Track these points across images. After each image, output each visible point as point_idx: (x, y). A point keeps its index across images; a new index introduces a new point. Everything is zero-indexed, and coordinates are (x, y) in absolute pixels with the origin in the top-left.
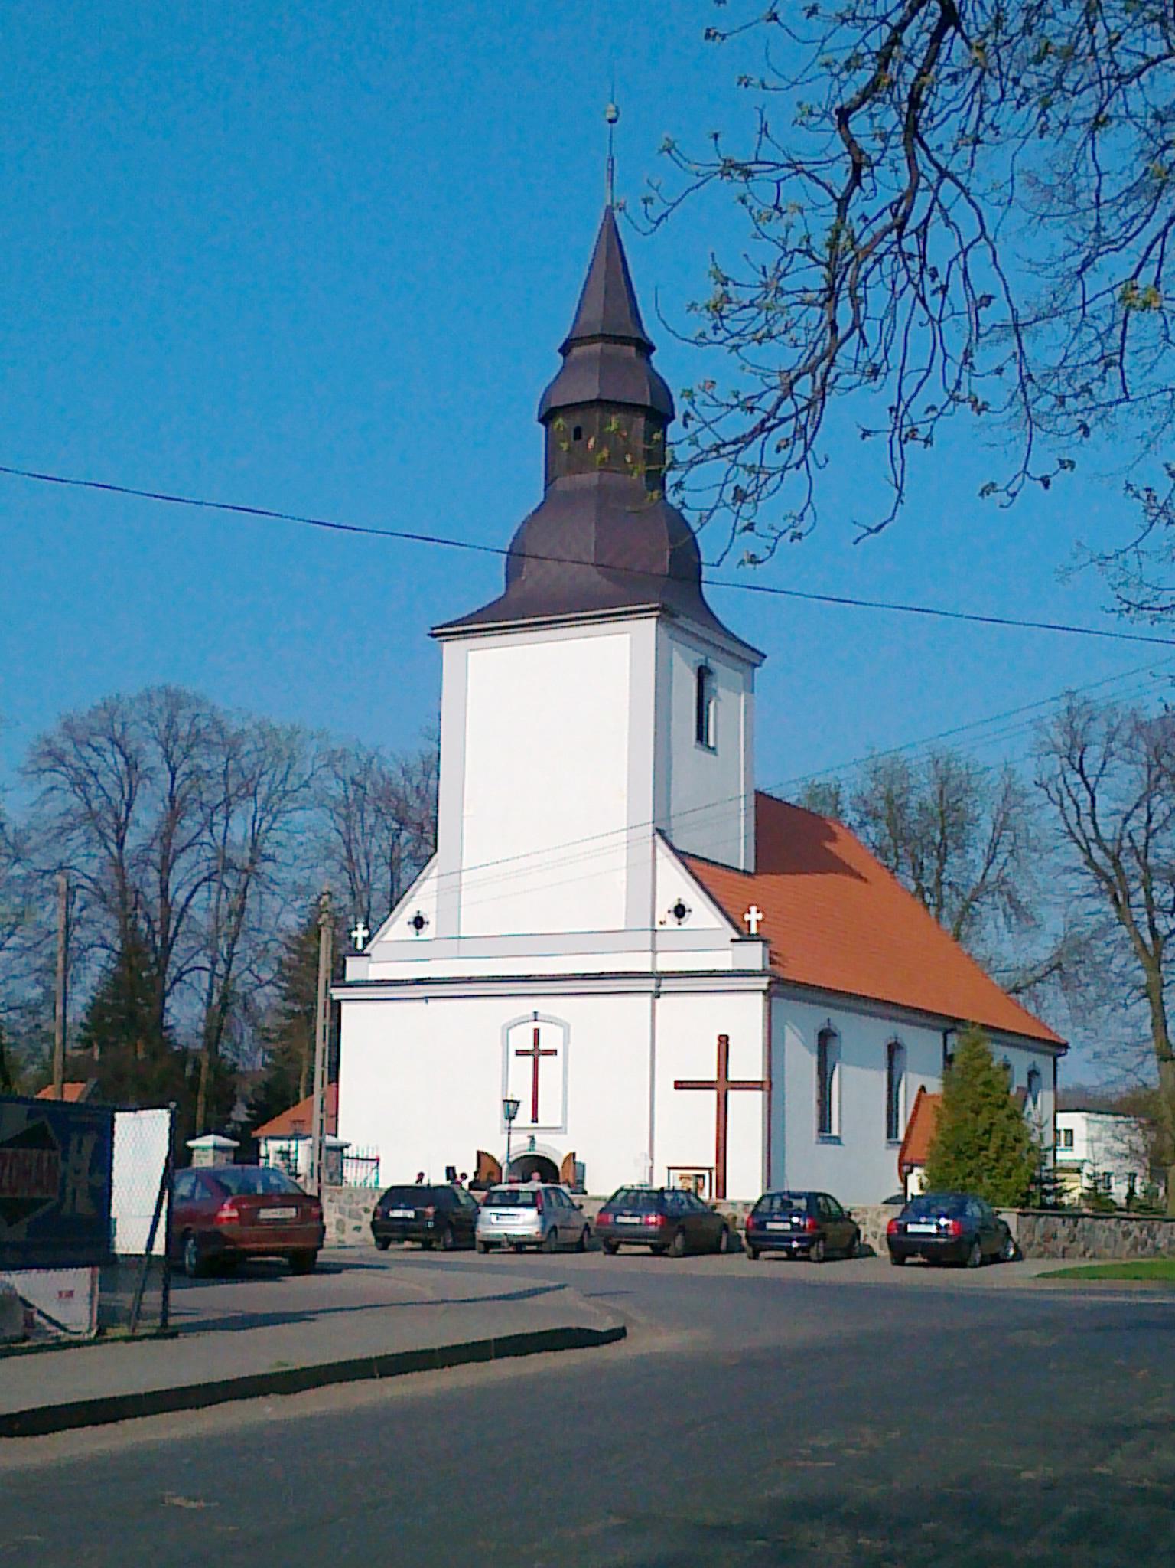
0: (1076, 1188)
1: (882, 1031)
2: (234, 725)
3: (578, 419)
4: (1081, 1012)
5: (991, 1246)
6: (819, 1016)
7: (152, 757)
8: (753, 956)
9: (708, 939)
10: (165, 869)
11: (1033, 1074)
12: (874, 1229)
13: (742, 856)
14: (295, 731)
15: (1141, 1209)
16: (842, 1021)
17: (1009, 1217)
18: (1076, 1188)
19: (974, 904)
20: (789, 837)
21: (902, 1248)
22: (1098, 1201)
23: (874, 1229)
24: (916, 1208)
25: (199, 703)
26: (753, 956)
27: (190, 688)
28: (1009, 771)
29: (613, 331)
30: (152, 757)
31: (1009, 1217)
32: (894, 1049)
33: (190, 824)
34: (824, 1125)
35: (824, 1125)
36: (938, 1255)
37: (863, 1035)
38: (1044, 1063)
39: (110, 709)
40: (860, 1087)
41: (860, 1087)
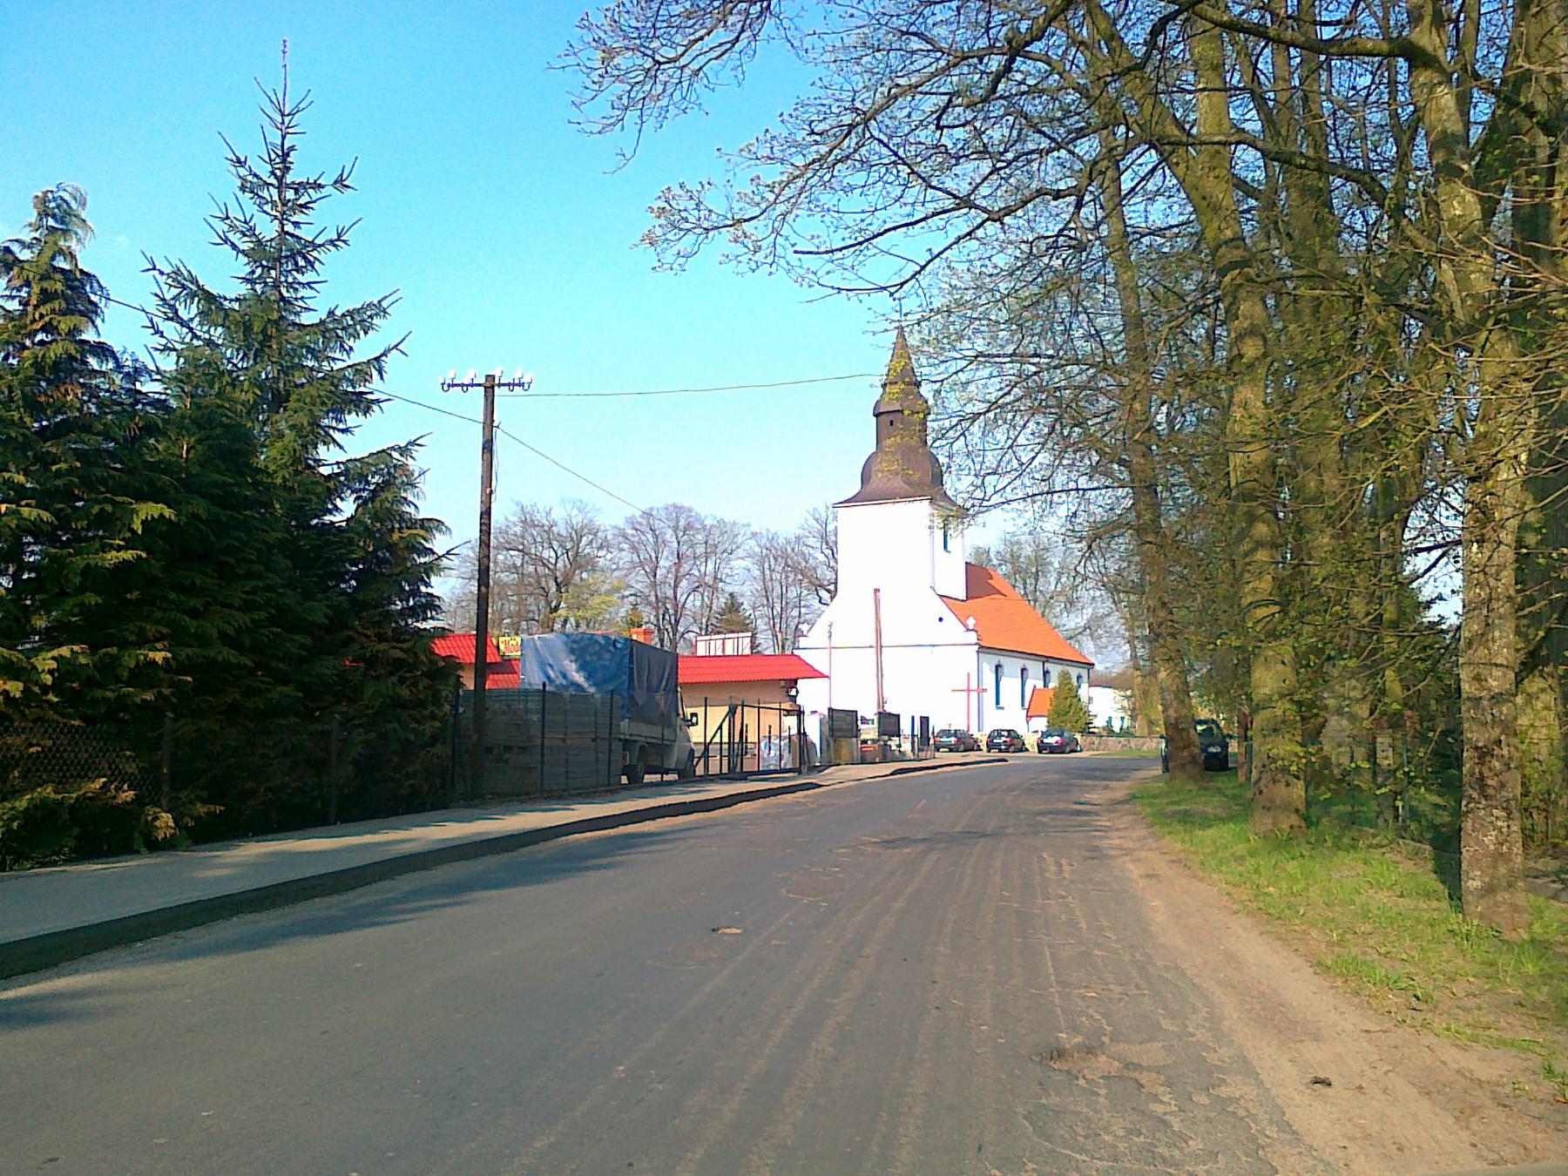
0: (1099, 722)
1: (1020, 663)
2: (708, 522)
3: (891, 417)
4: (1099, 649)
5: (1073, 746)
6: (995, 659)
7: (669, 535)
8: (973, 637)
9: (953, 629)
10: (676, 586)
11: (1079, 677)
12: (1031, 741)
13: (962, 595)
14: (735, 523)
15: (1125, 733)
16: (1004, 661)
17: (1078, 736)
18: (1099, 722)
19: (1116, 729)
20: (978, 578)
21: (1042, 747)
22: (1109, 729)
23: (1031, 741)
24: (1046, 734)
25: (690, 510)
26: (973, 637)
27: (686, 504)
28: (1109, 721)
29: (903, 379)
30: (669, 535)
31: (1078, 736)
32: (1023, 670)
33: (685, 568)
34: (998, 703)
35: (998, 703)
36: (1052, 750)
37: (1012, 666)
38: (1084, 673)
39: (648, 514)
40: (1010, 685)
41: (1010, 685)
